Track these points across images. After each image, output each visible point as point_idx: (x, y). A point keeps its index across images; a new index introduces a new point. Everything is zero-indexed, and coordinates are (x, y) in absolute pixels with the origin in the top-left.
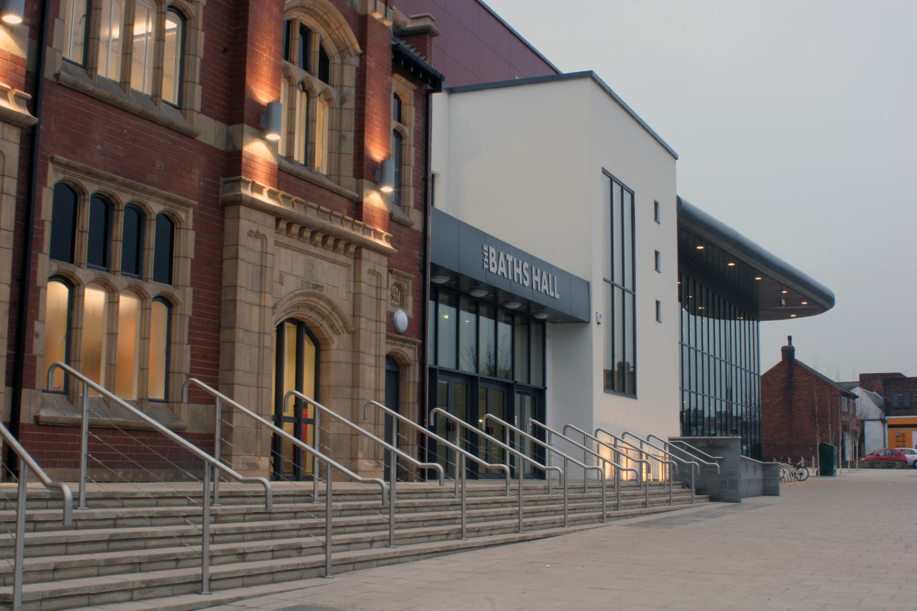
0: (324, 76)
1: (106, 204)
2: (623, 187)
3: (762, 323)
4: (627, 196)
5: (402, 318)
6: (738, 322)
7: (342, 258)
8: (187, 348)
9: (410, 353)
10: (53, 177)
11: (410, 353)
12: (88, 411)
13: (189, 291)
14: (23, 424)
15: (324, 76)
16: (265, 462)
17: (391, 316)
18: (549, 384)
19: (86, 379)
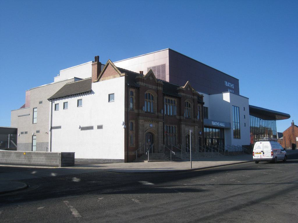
0: (190, 107)
1: (169, 127)
2: (237, 107)
3: (277, 121)
4: (238, 108)
5: (200, 133)
6: (253, 126)
7: (193, 127)
8: (135, 106)
9: (202, 137)
10: (165, 125)
11: (202, 137)
12: (166, 148)
13: (177, 134)
14: (76, 159)
15: (190, 107)
16: (185, 150)
17: (199, 133)
18: (225, 138)
19: (293, 160)
